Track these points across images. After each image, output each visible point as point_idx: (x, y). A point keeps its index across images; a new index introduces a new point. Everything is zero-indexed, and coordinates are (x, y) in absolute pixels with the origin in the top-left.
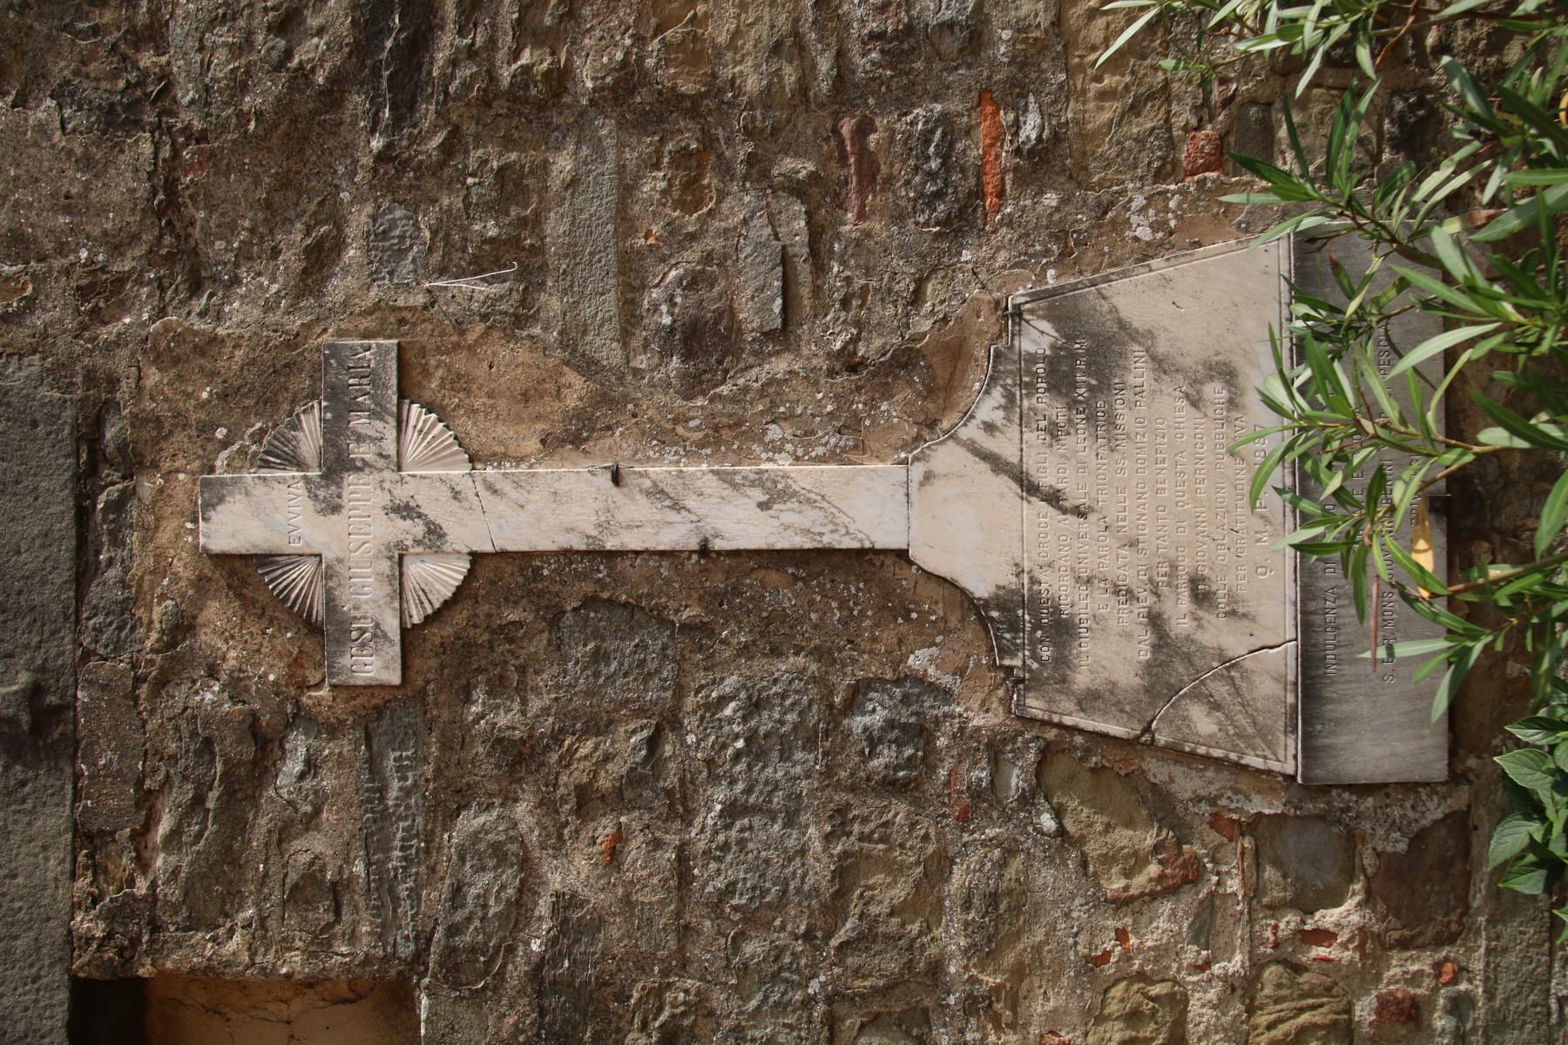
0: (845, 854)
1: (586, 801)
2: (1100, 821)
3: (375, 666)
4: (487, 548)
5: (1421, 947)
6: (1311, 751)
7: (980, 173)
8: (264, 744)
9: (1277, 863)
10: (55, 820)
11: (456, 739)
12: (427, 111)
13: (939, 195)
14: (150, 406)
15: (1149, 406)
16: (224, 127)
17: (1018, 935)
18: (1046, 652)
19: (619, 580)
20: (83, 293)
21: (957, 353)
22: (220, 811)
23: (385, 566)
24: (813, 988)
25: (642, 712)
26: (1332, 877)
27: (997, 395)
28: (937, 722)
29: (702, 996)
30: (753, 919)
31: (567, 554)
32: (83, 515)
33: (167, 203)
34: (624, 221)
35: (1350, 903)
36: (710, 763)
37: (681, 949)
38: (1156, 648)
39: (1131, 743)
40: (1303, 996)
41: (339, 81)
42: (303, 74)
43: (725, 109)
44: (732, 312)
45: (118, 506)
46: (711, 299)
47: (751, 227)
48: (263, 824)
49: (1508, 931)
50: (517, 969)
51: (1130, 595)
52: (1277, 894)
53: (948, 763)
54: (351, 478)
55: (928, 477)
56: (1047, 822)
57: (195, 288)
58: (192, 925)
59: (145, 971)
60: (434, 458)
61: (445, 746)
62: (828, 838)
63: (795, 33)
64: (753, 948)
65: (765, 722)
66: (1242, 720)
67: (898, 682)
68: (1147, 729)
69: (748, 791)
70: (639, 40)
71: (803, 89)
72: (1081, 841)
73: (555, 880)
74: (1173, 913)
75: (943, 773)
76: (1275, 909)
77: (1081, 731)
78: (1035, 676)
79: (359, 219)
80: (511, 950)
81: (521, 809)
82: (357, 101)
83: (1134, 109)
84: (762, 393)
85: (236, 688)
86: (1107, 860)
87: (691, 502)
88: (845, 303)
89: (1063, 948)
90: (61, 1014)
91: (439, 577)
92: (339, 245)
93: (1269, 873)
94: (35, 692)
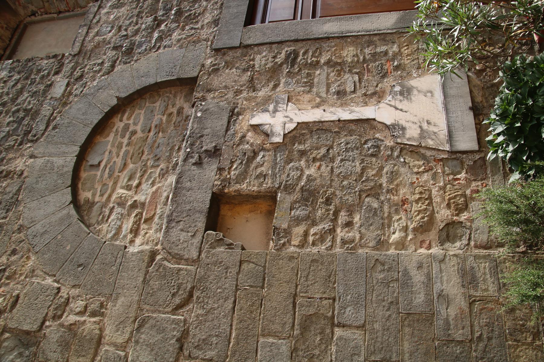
0: (363, 166)
1: (315, 160)
2: (412, 160)
4: (300, 121)
5: (478, 181)
6: (451, 145)
7: (387, 70)
8: (255, 154)
9: (447, 167)
10: (215, 167)
12: (296, 66)
13: (381, 73)
14: (243, 106)
15: (416, 97)
16: (262, 69)
17: (397, 179)
18: (401, 132)
19: (323, 126)
20: (235, 92)
21: (384, 92)
22: (245, 164)
23: (282, 125)
24: (357, 189)
25: (326, 146)
26: (459, 169)
27: (391, 96)
28: (381, 145)
29: (334, 192)
30: (345, 178)
31: (315, 122)
32: (229, 122)
33: (251, 80)
34: (327, 78)
35: (463, 173)
36: (338, 153)
37: (331, 183)
38: (421, 131)
39: (417, 146)
40: (455, 190)
42: (277, 63)
43: (345, 64)
44: (345, 89)
45: (235, 120)
46: (342, 88)
47: (349, 80)
48: (253, 166)
49: (496, 177)
50: (298, 188)
51: (416, 123)
52: (448, 172)
53: (383, 151)
54: (278, 113)
55: (379, 108)
56: (402, 160)
57: (254, 91)
58: (236, 183)
59: (226, 191)
60: (293, 110)
61: (289, 152)
62: (360, 164)
63: (357, 54)
64: (345, 183)
65: (349, 146)
66: (438, 142)
67: (373, 139)
68: (420, 144)
69: (345, 157)
70: (331, 56)
71: (358, 61)
72: (409, 163)
73: (307, 172)
74: (427, 175)
75: (382, 153)
76: (448, 175)
77: (408, 145)
78: (399, 136)
79: (283, 81)
80: (297, 185)
81: (302, 162)
82: (285, 66)
83: (413, 61)
84: (350, 99)
85: (252, 145)
86: (414, 166)
87: (337, 113)
88: (365, 87)
89: (406, 182)
90: (209, 198)
91: (291, 126)
92: (279, 84)
93: (446, 168)
94: (216, 146)
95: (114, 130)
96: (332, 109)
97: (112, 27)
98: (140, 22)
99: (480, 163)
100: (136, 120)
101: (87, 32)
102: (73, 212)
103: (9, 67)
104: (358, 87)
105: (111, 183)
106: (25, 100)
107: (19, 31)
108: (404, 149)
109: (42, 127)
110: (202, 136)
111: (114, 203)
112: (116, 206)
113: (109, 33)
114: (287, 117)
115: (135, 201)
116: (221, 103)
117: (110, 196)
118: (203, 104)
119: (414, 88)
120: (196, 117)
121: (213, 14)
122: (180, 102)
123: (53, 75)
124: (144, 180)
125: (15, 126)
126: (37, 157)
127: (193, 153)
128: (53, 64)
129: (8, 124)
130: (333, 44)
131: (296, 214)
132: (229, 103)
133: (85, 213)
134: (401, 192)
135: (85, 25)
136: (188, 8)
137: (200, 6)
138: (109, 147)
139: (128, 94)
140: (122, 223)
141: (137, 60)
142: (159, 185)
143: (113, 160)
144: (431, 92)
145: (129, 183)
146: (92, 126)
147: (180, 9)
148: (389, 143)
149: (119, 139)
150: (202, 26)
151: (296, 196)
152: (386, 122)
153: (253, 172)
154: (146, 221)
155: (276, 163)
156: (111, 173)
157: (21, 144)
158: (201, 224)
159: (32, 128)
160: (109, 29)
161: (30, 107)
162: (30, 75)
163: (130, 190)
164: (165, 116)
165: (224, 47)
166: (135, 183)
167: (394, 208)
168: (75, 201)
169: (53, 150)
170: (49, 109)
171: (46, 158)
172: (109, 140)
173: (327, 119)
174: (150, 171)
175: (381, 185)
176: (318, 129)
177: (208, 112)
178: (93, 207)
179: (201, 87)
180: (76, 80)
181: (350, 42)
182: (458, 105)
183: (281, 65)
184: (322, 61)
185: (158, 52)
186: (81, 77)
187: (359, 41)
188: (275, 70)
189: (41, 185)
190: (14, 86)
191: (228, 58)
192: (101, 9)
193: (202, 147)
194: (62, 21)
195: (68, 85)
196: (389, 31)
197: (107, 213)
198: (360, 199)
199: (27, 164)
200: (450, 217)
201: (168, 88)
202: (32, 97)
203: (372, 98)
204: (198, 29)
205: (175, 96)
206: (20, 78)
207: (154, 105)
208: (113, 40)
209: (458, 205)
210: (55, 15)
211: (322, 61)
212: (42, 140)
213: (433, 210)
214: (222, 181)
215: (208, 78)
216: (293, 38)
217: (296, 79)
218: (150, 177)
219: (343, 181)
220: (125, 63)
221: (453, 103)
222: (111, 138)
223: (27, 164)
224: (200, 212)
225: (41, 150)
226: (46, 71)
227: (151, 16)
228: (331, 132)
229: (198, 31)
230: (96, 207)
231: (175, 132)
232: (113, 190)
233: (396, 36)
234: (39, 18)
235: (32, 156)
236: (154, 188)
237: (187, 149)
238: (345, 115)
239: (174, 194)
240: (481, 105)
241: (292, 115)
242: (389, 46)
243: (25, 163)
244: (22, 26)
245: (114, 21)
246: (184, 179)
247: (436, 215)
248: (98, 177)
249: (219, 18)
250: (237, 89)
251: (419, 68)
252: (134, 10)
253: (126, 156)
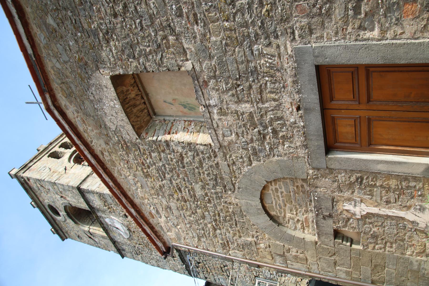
3: (359, 217)
11: (365, 221)
12: (363, 185)
32: (333, 204)
34: (381, 193)
41: (354, 182)
42: (351, 181)
47: (392, 196)
48: (349, 224)
50: (370, 234)
57: (342, 192)
71: (398, 188)
79: (356, 191)
92: (355, 191)
110: (321, 208)
147: (273, 128)
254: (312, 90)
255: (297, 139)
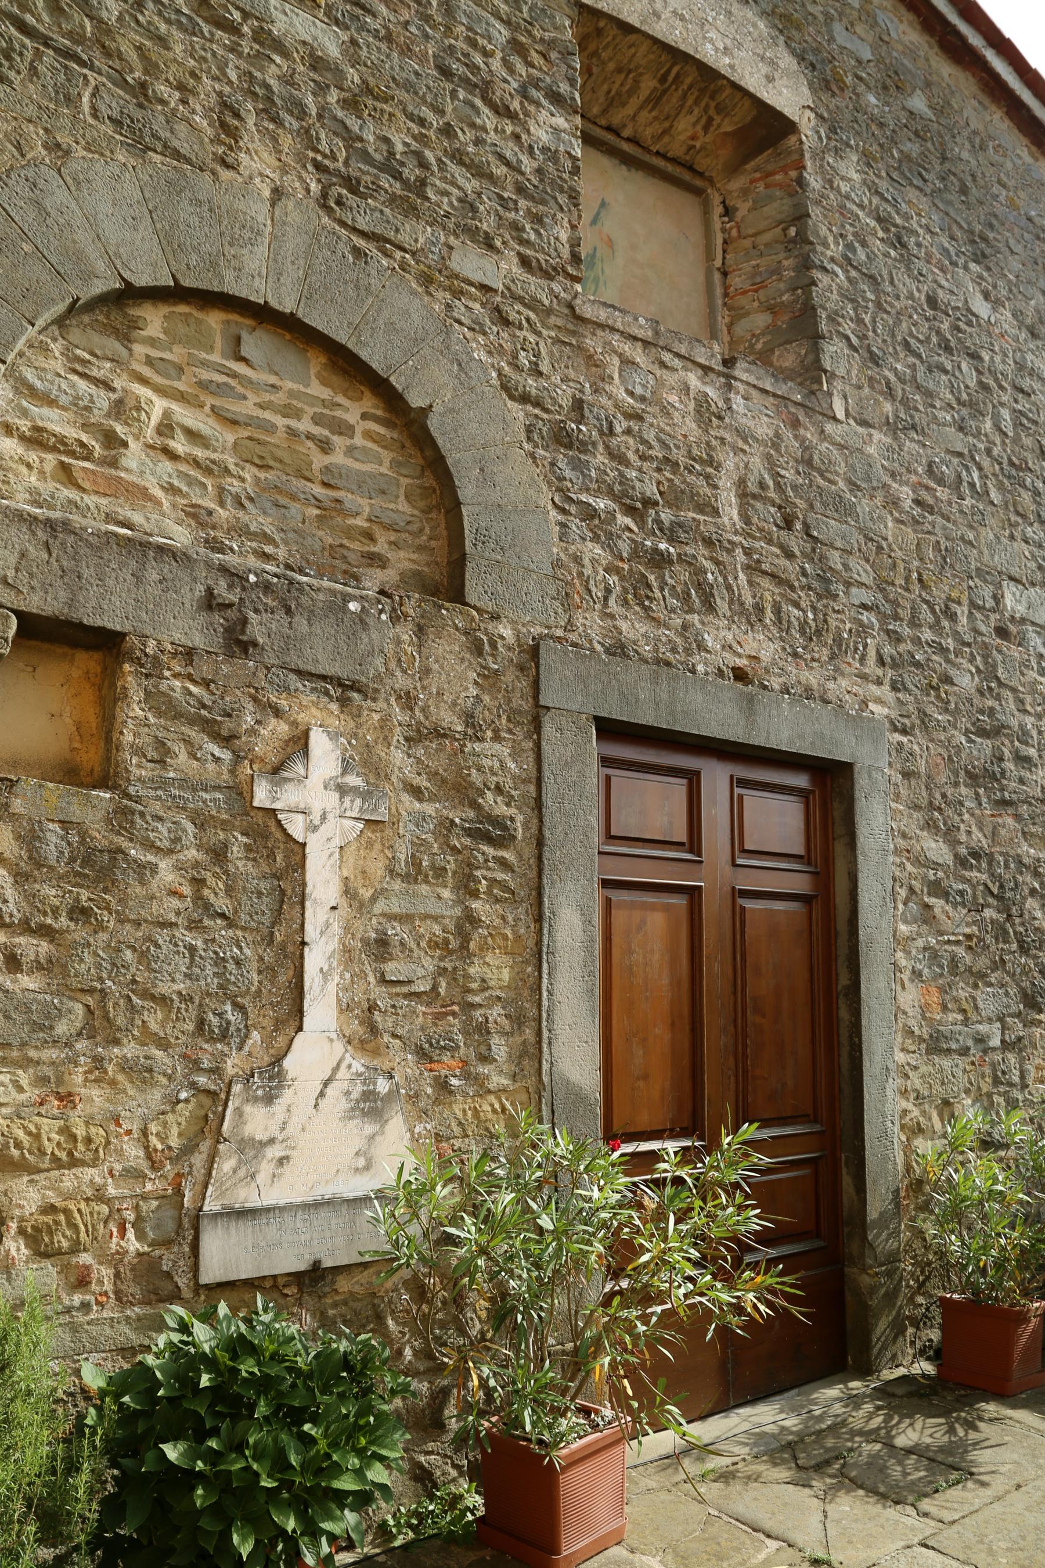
1: (198, 883)
6: (215, 1216)
8: (227, 740)
9: (158, 1207)
10: (198, 641)
12: (467, 841)
15: (358, 1131)
21: (376, 1053)
22: (200, 716)
23: (302, 806)
24: (109, 983)
25: (236, 912)
26: (151, 1235)
27: (362, 1069)
30: (143, 956)
31: (304, 885)
32: (324, 678)
33: (439, 733)
34: (426, 917)
35: (138, 1245)
36: (213, 940)
42: (482, 794)
43: (463, 959)
45: (327, 693)
46: (396, 951)
47: (418, 969)
48: (192, 733)
50: (121, 841)
54: (337, 795)
55: (331, 1040)
56: (183, 1095)
57: (407, 739)
58: (147, 692)
59: (127, 667)
60: (343, 833)
61: (224, 822)
62: (180, 993)
65: (231, 966)
71: (469, 991)
72: (173, 1111)
73: (164, 865)
75: (206, 1046)
79: (430, 809)
80: (131, 840)
81: (194, 852)
82: (471, 814)
83: (460, 1124)
85: (252, 732)
90: (110, 626)
91: (296, 827)
92: (420, 800)
93: (155, 1204)
94: (255, 645)
95: (340, 399)
96: (336, 928)
97: (643, 399)
98: (646, 465)
99: (167, 1287)
100: (360, 448)
101: (635, 338)
102: (99, 287)
103: (562, 148)
104: (398, 990)
105: (181, 386)
106: (453, 184)
107: (687, 176)
108: (214, 1101)
109: (362, 223)
110: (288, 611)
111: (124, 390)
112: (113, 396)
113: (627, 391)
114: (324, 818)
115: (125, 444)
116: (378, 661)
117: (144, 381)
118: (383, 617)
119: (382, 1126)
120: (346, 598)
121: (642, 643)
122: (403, 560)
123: (519, 254)
124: (184, 467)
125: (377, 157)
126: (273, 205)
127: (244, 589)
128: (554, 254)
129: (386, 140)
130: (522, 931)
131: (48, 834)
132: (378, 677)
133: (101, 318)
134: (95, 1092)
135: (657, 333)
136: (670, 581)
137: (673, 610)
138: (289, 385)
139: (435, 434)
140: (63, 408)
141: (534, 458)
142: (166, 504)
143: (249, 394)
144: (367, 1167)
145: (178, 431)
146: (350, 346)
147: (671, 562)
148: (232, 1065)
149: (310, 411)
150: (612, 616)
151: (100, 836)
152: (289, 1056)
153: (174, 733)
154: (65, 467)
155: (194, 790)
156: (213, 387)
157: (318, 167)
158: (35, 603)
159: (364, 197)
160: (639, 390)
161: (430, 194)
162: (532, 198)
163: (159, 432)
164: (366, 525)
165: (542, 669)
166: (179, 445)
167: (51, 1074)
168: (130, 294)
169: (290, 246)
170: (416, 241)
171: (269, 228)
172: (312, 385)
173: (308, 914)
174: (209, 482)
175: (117, 1042)
176: (283, 892)
177: (359, 627)
178: (117, 339)
179: (434, 611)
180: (498, 309)
181: (523, 971)
182: (328, 1234)
183: (474, 805)
184: (475, 905)
185: (550, 506)
186: (506, 322)
187: (526, 993)
188: (463, 792)
189: (186, 212)
190: (501, 157)
191: (509, 677)
192: (700, 372)
193: (256, 611)
194: (701, 278)
195: (485, 288)
196: (545, 1066)
197: (95, 373)
198: (82, 990)
199: (257, 180)
200: (17, 1212)
201: (445, 533)
202: (460, 200)
203: (361, 1023)
204: (606, 605)
205: (420, 549)
206: (523, 174)
207: (402, 498)
208: (604, 400)
209: (50, 1233)
210: (718, 263)
211: (475, 905)
212: (326, 220)
213: (40, 1171)
214: (155, 657)
215: (457, 629)
216: (547, 834)
217: (431, 840)
218: (191, 482)
219: (134, 949)
220: (529, 430)
221: (333, 1222)
222: (317, 390)
223: (257, 180)
224: (71, 602)
225: (295, 217)
226: (533, 237)
227: (661, 493)
228: (273, 924)
229: (598, 606)
230: (117, 345)
231: (317, 546)
232: (160, 391)
233: (531, 1082)
234: (717, 223)
235: (277, 193)
236: (158, 493)
237: (256, 575)
238: (316, 960)
239: (129, 539)
240: (327, 1289)
241: (326, 830)
242: (505, 1068)
243: (261, 174)
244: (698, 183)
245: (659, 402)
246: (168, 567)
247: (26, 1179)
248: (204, 355)
249: (628, 657)
250: (416, 698)
251: (438, 1137)
252: (683, 451)
253: (259, 427)
254: (801, 737)
255: (642, 630)
